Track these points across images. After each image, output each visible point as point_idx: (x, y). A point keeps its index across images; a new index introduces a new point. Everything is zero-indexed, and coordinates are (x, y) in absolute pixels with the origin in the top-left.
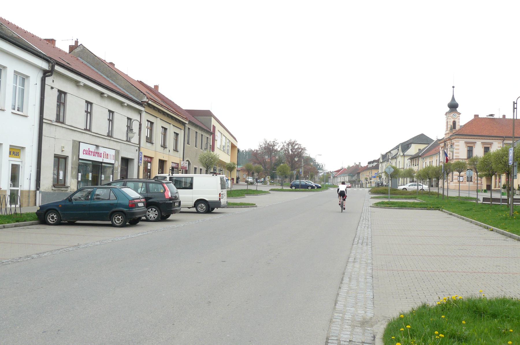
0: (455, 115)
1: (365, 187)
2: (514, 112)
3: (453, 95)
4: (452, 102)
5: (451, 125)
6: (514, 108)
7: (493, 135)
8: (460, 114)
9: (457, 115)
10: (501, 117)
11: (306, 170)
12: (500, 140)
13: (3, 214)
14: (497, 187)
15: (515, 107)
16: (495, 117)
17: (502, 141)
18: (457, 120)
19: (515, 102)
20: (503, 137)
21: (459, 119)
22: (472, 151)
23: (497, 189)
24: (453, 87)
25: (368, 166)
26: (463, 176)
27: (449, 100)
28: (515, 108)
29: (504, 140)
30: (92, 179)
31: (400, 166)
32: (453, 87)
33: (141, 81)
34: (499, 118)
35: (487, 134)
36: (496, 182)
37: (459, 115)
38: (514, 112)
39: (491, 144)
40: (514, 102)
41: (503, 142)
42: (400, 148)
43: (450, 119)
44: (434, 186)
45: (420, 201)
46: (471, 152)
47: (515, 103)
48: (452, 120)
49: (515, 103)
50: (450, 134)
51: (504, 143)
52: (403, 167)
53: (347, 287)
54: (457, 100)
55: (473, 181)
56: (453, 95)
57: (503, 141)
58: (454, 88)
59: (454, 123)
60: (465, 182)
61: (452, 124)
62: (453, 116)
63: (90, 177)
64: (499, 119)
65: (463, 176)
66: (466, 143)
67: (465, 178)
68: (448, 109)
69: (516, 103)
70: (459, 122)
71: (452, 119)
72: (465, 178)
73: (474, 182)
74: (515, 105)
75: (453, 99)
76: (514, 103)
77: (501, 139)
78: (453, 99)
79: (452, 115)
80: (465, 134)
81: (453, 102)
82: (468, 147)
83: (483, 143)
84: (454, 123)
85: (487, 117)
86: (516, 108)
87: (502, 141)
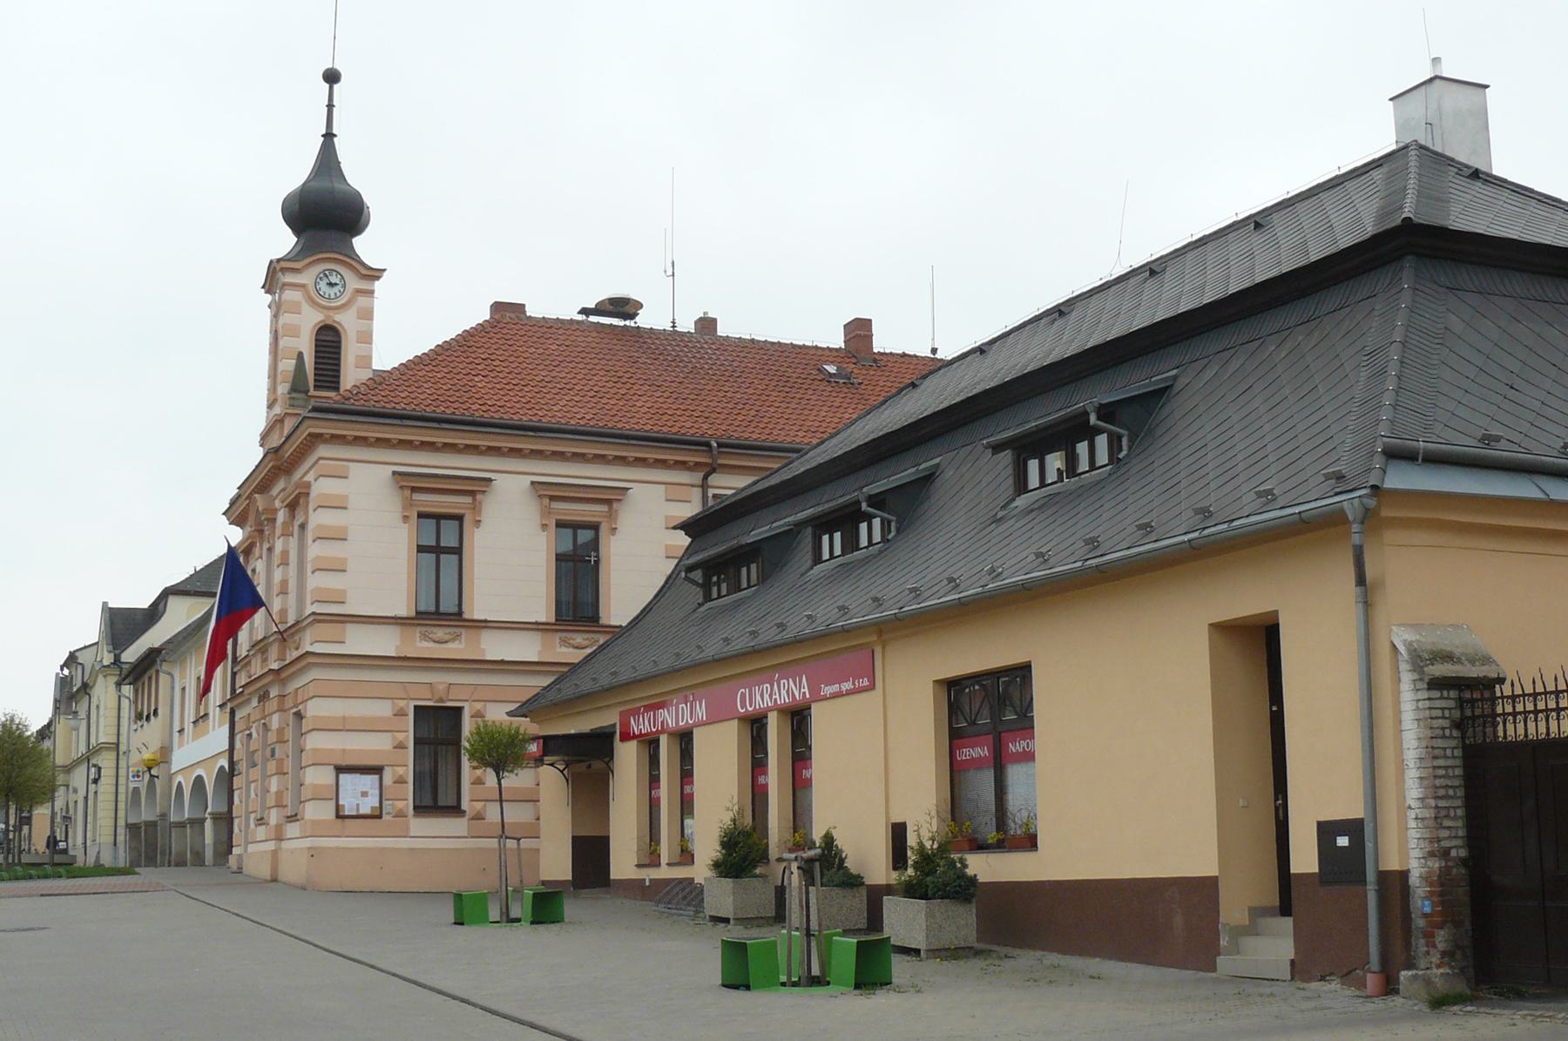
0: (334, 279)
1: (992, 836)
3: (329, 136)
4: (313, 184)
7: (625, 426)
8: (375, 274)
9: (353, 283)
10: (687, 325)
12: (681, 465)
14: (664, 859)
16: (644, 320)
17: (697, 477)
18: (347, 322)
20: (708, 445)
21: (367, 315)
22: (458, 551)
23: (664, 873)
24: (332, 77)
26: (377, 770)
27: (296, 172)
29: (714, 470)
31: (101, 734)
32: (332, 77)
34: (668, 327)
35: (582, 416)
36: (654, 804)
37: (363, 285)
39: (611, 498)
41: (704, 486)
43: (296, 309)
44: (188, 863)
46: (448, 561)
48: (308, 320)
50: (286, 422)
51: (711, 492)
52: (115, 741)
53: (1083, 544)
54: (357, 174)
55: (465, 805)
56: (329, 136)
57: (705, 478)
58: (336, 87)
59: (329, 342)
60: (401, 814)
61: (306, 345)
62: (323, 285)
64: (673, 336)
65: (377, 770)
66: (409, 483)
67: (401, 781)
68: (285, 240)
70: (366, 338)
71: (306, 308)
72: (401, 781)
73: (479, 817)
75: (327, 159)
77: (691, 459)
78: (327, 159)
79: (307, 278)
80: (400, 408)
81: (324, 184)
82: (421, 515)
83: (547, 493)
84: (329, 342)
85: (581, 317)
87: (697, 477)
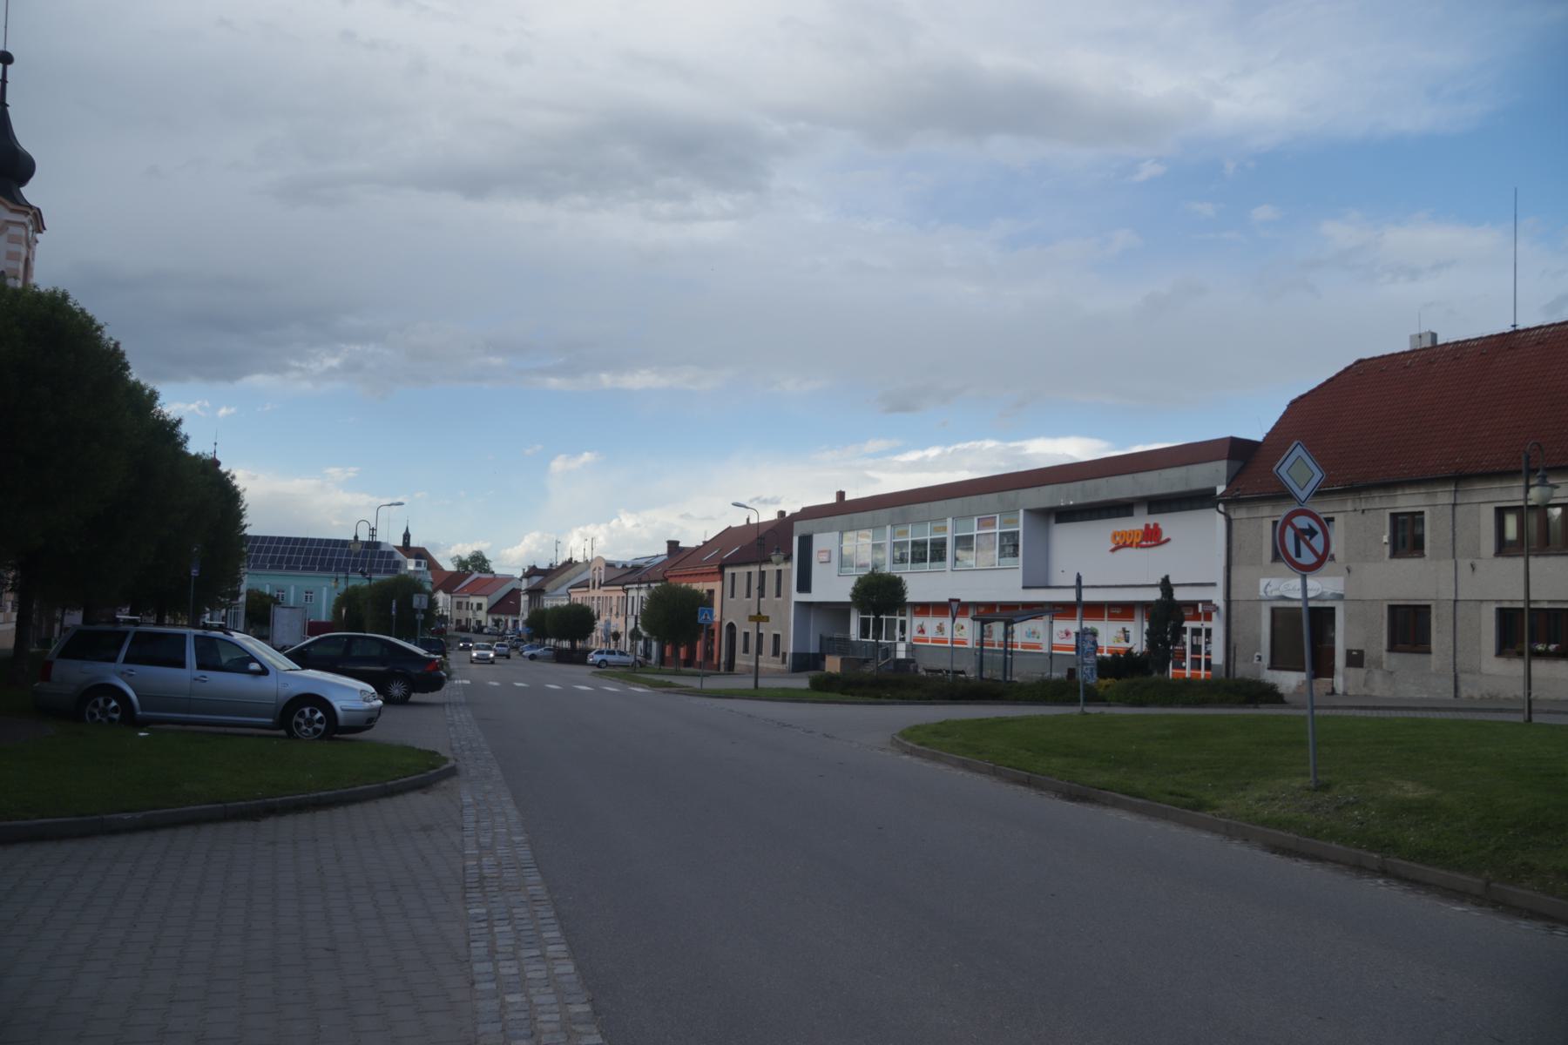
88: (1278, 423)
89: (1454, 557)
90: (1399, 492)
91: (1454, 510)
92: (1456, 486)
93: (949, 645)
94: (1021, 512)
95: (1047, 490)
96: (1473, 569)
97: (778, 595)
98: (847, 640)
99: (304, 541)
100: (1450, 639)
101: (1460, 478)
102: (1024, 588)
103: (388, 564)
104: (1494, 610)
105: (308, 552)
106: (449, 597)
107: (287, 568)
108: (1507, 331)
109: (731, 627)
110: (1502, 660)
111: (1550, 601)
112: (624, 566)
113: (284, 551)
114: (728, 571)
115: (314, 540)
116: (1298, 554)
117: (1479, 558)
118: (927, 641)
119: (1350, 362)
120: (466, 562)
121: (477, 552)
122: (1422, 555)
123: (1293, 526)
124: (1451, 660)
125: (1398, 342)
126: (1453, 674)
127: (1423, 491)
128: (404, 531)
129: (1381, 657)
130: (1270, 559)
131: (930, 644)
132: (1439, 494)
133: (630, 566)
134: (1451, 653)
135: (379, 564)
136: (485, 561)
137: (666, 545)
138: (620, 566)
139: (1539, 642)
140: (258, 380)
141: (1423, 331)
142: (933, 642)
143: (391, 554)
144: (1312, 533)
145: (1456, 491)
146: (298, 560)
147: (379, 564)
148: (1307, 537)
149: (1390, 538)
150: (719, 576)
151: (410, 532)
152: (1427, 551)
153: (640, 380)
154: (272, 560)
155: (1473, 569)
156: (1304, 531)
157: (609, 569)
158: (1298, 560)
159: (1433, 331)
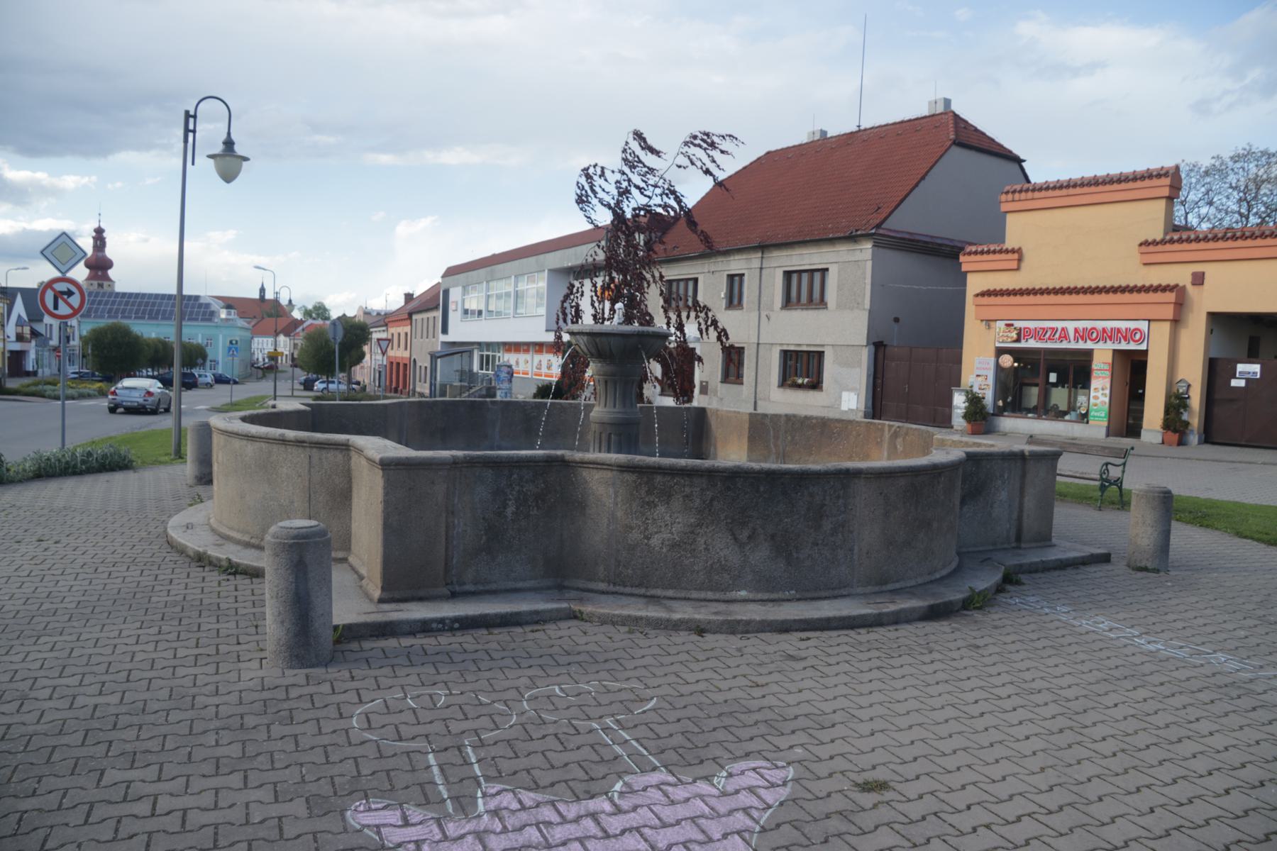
2: (186, 141)
5: (193, 164)
6: (187, 131)
11: (455, 543)
13: (587, 283)
15: (191, 127)
19: (192, 113)
25: (1013, 365)
28: (191, 131)
30: (1258, 363)
33: (564, 297)
38: (186, 141)
40: (187, 113)
42: (320, 322)
45: (787, 665)
47: (191, 116)
49: (191, 116)
63: (917, 459)
69: (195, 117)
74: (191, 120)
76: (187, 115)
86: (194, 131)
88: (703, 198)
89: (759, 310)
90: (732, 258)
91: (761, 272)
92: (763, 253)
93: (529, 376)
94: (546, 271)
95: (559, 254)
96: (769, 319)
97: (434, 337)
98: (471, 371)
99: (137, 295)
100: (754, 374)
101: (763, 247)
102: (547, 331)
103: (204, 314)
104: (778, 351)
105: (140, 304)
106: (288, 339)
107: (135, 318)
108: (854, 130)
109: (415, 360)
110: (781, 390)
111: (808, 345)
112: (379, 314)
113: (120, 304)
114: (414, 317)
115: (165, 295)
116: (56, 307)
117: (773, 311)
118: (541, 375)
119: (761, 153)
120: (310, 311)
121: (319, 303)
122: (743, 308)
123: (53, 290)
124: (753, 389)
125: (797, 136)
126: (753, 400)
127: (744, 257)
128: (260, 286)
129: (717, 387)
130: (780, 306)
131: (521, 375)
132: (732, 262)
133: (383, 313)
134: (754, 384)
135: (198, 313)
136: (325, 310)
137: (403, 297)
138: (375, 314)
139: (801, 376)
140: (126, 157)
141: (816, 129)
142: (546, 376)
143: (208, 305)
144: (70, 293)
145: (762, 258)
146: (131, 311)
147: (198, 313)
148: (65, 297)
149: (726, 294)
150: (409, 321)
151: (265, 286)
152: (745, 306)
153: (452, 157)
154: (110, 311)
155: (769, 319)
156: (62, 293)
157: (366, 316)
158: (56, 312)
159: (824, 129)
